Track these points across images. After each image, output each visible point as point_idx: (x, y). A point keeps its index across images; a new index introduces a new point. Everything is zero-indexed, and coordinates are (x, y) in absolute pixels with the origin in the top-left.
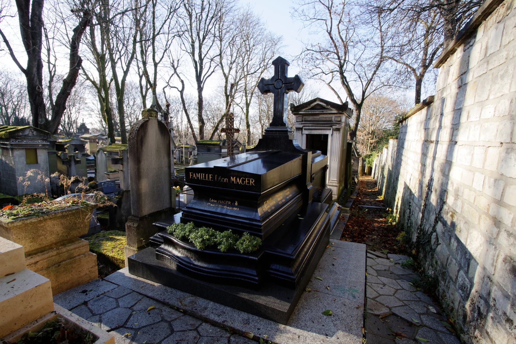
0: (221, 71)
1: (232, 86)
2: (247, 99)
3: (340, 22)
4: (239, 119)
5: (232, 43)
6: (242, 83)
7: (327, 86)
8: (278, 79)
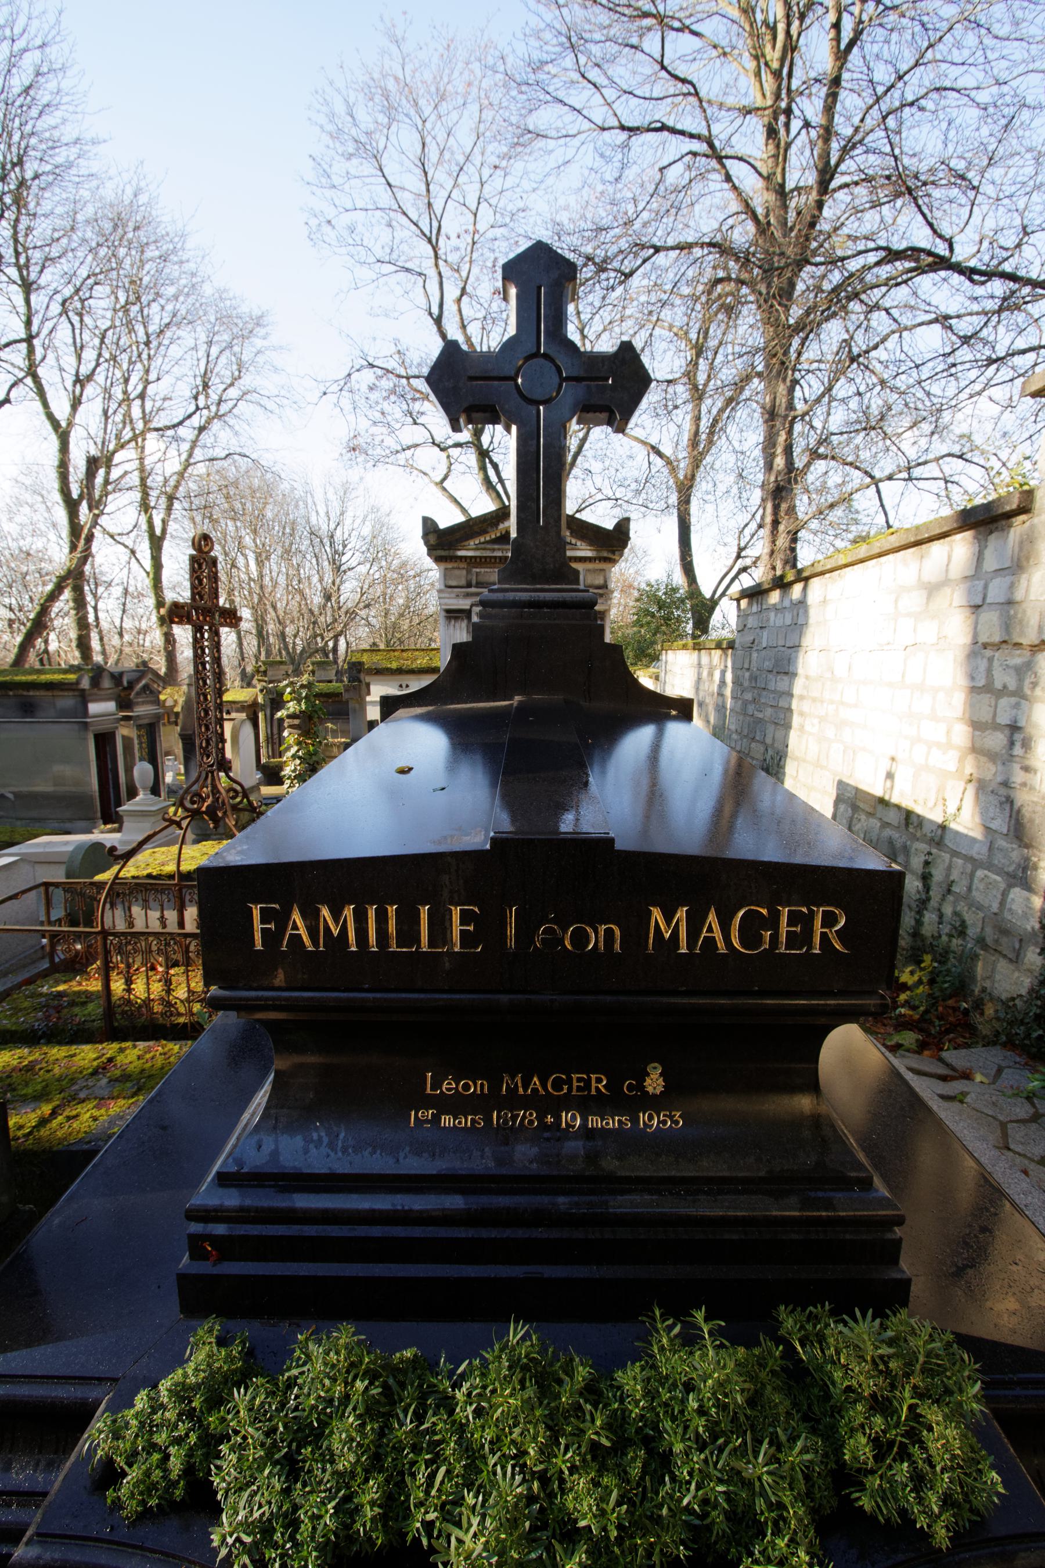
0: (38, 405)
1: (93, 464)
2: (878, 264)
3: (462, 295)
4: (117, 591)
5: (74, 306)
6: (125, 460)
7: (437, 492)
8: (536, 354)
